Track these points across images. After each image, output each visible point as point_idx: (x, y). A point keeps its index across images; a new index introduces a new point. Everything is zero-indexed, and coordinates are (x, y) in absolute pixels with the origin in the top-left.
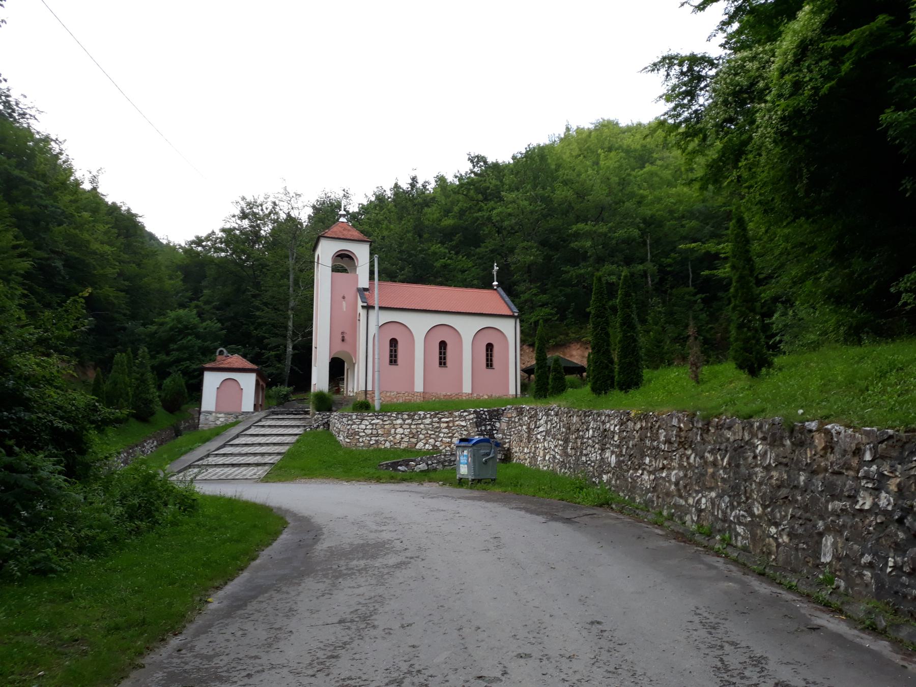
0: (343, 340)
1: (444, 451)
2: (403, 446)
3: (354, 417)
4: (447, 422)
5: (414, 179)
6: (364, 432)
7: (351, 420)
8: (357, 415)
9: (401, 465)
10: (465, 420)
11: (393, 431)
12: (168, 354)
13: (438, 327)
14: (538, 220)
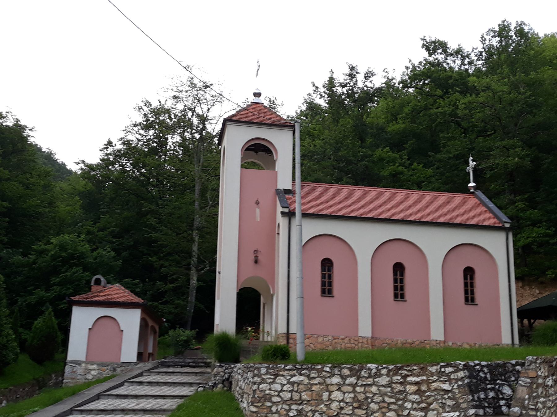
0: (256, 262)
3: (263, 371)
4: (417, 383)
6: (279, 396)
8: (268, 368)
10: (450, 380)
11: (325, 395)
12: (48, 290)
13: (391, 243)
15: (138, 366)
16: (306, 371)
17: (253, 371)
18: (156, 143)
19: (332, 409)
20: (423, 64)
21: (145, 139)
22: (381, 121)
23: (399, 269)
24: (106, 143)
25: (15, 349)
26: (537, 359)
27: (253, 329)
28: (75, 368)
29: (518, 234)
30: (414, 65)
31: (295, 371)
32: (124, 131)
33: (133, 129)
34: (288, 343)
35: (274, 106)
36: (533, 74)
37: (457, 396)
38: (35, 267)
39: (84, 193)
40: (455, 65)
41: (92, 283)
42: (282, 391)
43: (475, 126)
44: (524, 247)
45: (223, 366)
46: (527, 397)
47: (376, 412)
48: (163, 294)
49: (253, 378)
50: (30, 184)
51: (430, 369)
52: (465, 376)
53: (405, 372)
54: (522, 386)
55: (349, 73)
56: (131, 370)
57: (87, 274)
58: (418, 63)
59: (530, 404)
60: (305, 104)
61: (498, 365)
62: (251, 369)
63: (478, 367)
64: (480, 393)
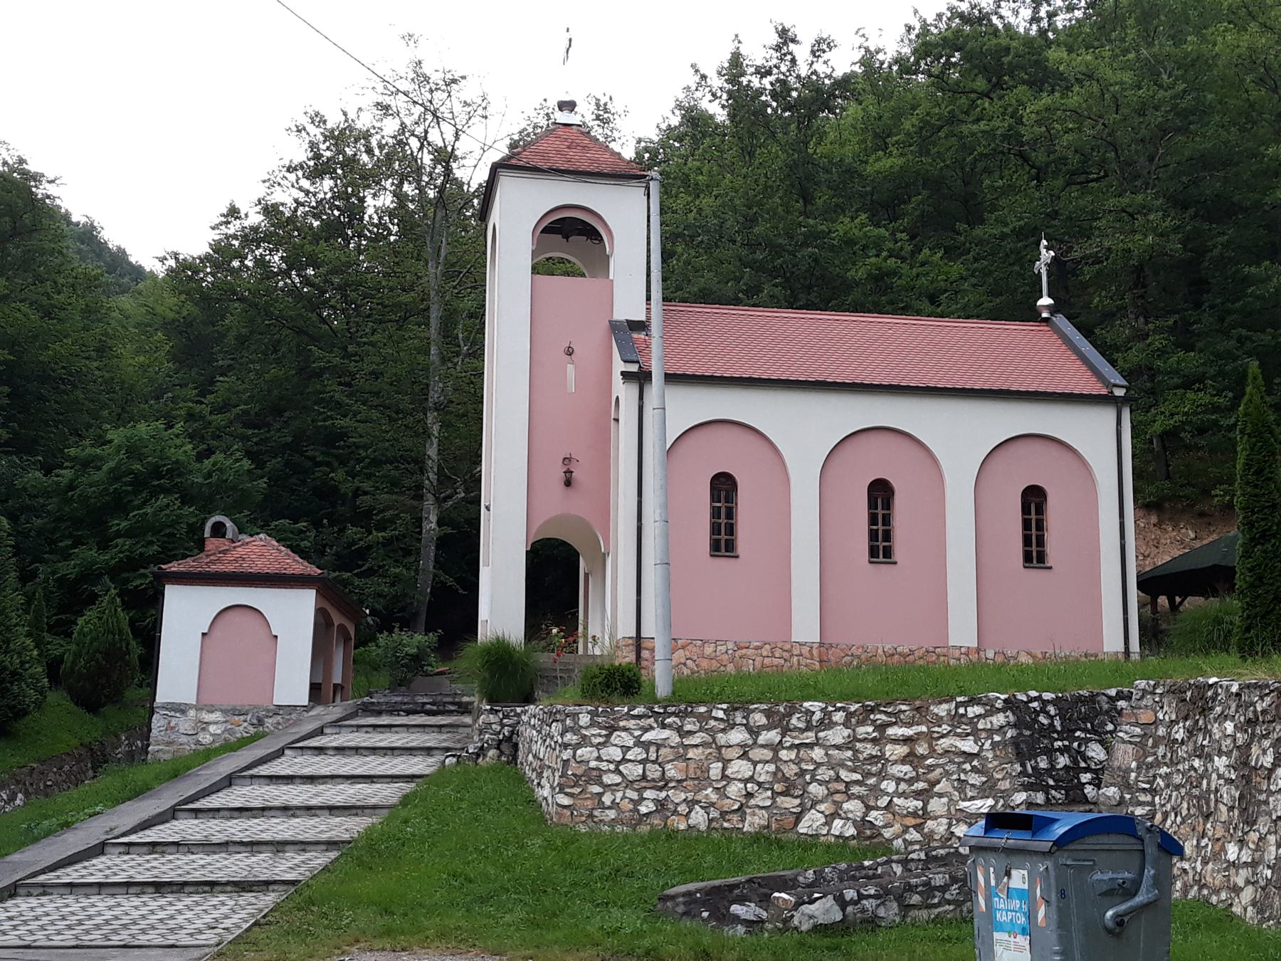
0: (568, 483)
1: (898, 843)
2: (754, 821)
3: (584, 720)
4: (907, 740)
5: (786, 37)
7: (570, 730)
8: (593, 714)
9: (741, 900)
10: (975, 733)
12: (104, 545)
13: (862, 438)
14: (1163, 130)
15: (312, 713)
16: (675, 719)
17: (563, 721)
18: (338, 208)
19: (728, 798)
20: (944, 19)
21: (313, 199)
22: (849, 151)
23: (881, 493)
24: (225, 211)
25: (38, 681)
26: (1155, 687)
27: (561, 630)
28: (173, 719)
29: (1150, 407)
30: (925, 21)
31: (652, 719)
32: (264, 182)
33: (284, 177)
34: (638, 657)
35: (606, 116)
36: (1191, 43)
37: (990, 765)
38: (73, 496)
39: (177, 323)
40: (1018, 20)
41: (207, 534)
42: (624, 760)
43: (1063, 160)
44: (1169, 436)
45: (497, 711)
46: (1134, 765)
47: (821, 802)
48: (363, 554)
49: (562, 735)
50: (53, 306)
51: (936, 711)
52: (1008, 724)
53: (883, 717)
54: (1124, 742)
55: (775, 43)
56: (297, 722)
57: (191, 510)
58: (935, 17)
59: (1140, 779)
60: (677, 112)
61: (1079, 700)
62: (558, 717)
63: (1035, 704)
64: (1039, 759)
